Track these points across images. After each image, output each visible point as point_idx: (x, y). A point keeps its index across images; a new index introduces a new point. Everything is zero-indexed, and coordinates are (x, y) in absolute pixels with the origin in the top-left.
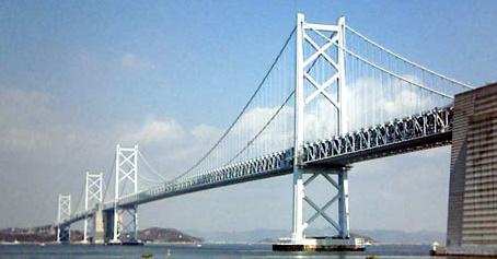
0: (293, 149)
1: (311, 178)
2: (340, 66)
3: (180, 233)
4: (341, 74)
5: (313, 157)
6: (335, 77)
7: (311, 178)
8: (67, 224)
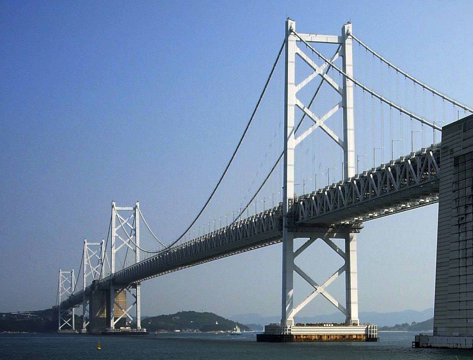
3: (220, 319)
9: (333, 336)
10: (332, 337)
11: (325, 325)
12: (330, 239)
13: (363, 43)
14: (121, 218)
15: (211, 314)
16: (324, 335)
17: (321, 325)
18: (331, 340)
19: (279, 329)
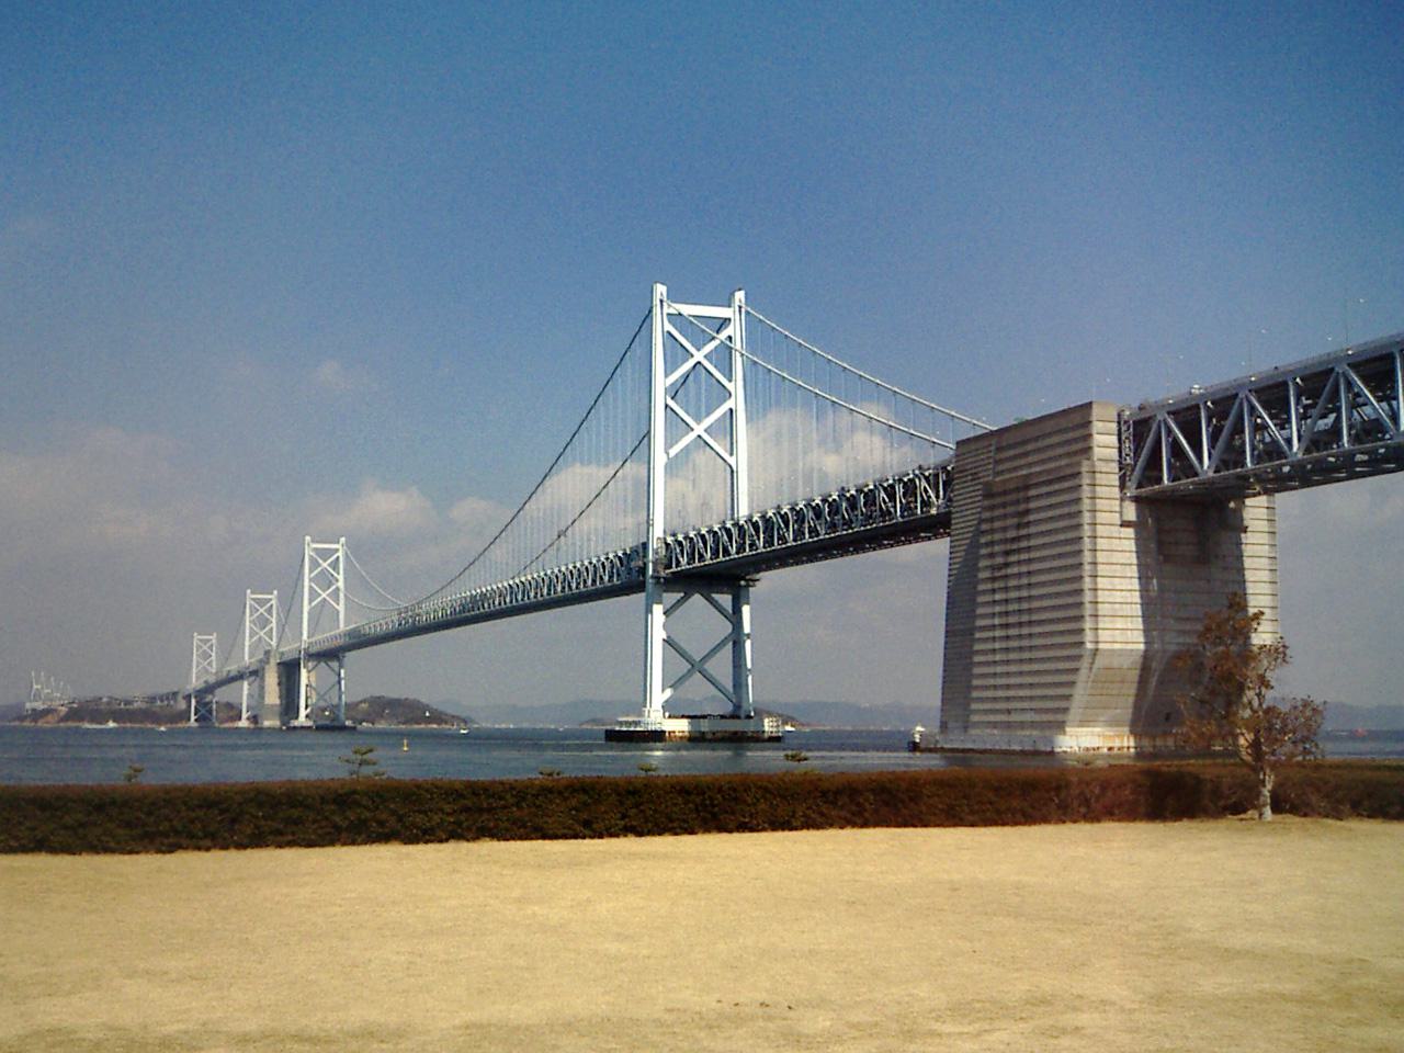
3: (426, 707)
4: (737, 402)
6: (724, 408)
8: (210, 689)
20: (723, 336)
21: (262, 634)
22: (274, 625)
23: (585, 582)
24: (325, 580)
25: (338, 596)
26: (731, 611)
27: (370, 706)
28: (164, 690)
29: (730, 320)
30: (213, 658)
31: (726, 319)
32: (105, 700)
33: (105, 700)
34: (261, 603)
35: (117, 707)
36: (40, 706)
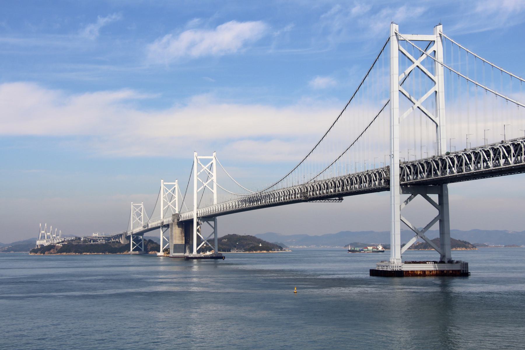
0: (163, 222)
1: (167, 230)
2: (440, 77)
3: (260, 241)
4: (440, 86)
5: (439, 173)
6: (432, 91)
7: (167, 230)
8: (141, 233)
9: (434, 272)
10: (433, 272)
11: (427, 263)
12: (428, 195)
13: (470, 78)
14: (172, 206)
15: (234, 234)
16: (427, 271)
17: (425, 262)
18: (432, 274)
19: (392, 267)
20: (430, 51)
21: (170, 204)
22: (176, 199)
23: (499, 342)
24: (207, 177)
25: (213, 185)
26: (438, 203)
27: (228, 241)
28: (115, 233)
29: (434, 41)
30: (142, 215)
31: (432, 41)
32: (82, 239)
33: (82, 239)
34: (169, 187)
35: (89, 243)
36: (45, 243)
